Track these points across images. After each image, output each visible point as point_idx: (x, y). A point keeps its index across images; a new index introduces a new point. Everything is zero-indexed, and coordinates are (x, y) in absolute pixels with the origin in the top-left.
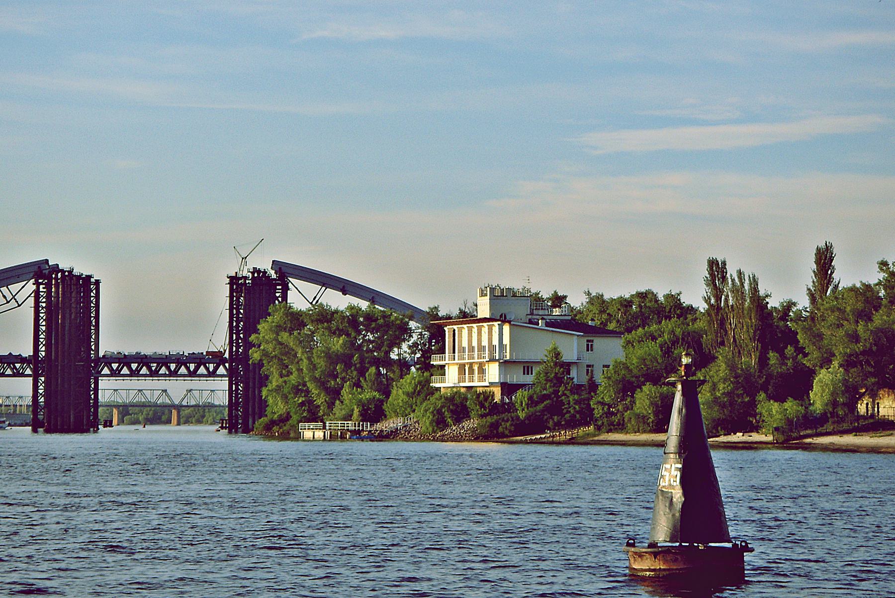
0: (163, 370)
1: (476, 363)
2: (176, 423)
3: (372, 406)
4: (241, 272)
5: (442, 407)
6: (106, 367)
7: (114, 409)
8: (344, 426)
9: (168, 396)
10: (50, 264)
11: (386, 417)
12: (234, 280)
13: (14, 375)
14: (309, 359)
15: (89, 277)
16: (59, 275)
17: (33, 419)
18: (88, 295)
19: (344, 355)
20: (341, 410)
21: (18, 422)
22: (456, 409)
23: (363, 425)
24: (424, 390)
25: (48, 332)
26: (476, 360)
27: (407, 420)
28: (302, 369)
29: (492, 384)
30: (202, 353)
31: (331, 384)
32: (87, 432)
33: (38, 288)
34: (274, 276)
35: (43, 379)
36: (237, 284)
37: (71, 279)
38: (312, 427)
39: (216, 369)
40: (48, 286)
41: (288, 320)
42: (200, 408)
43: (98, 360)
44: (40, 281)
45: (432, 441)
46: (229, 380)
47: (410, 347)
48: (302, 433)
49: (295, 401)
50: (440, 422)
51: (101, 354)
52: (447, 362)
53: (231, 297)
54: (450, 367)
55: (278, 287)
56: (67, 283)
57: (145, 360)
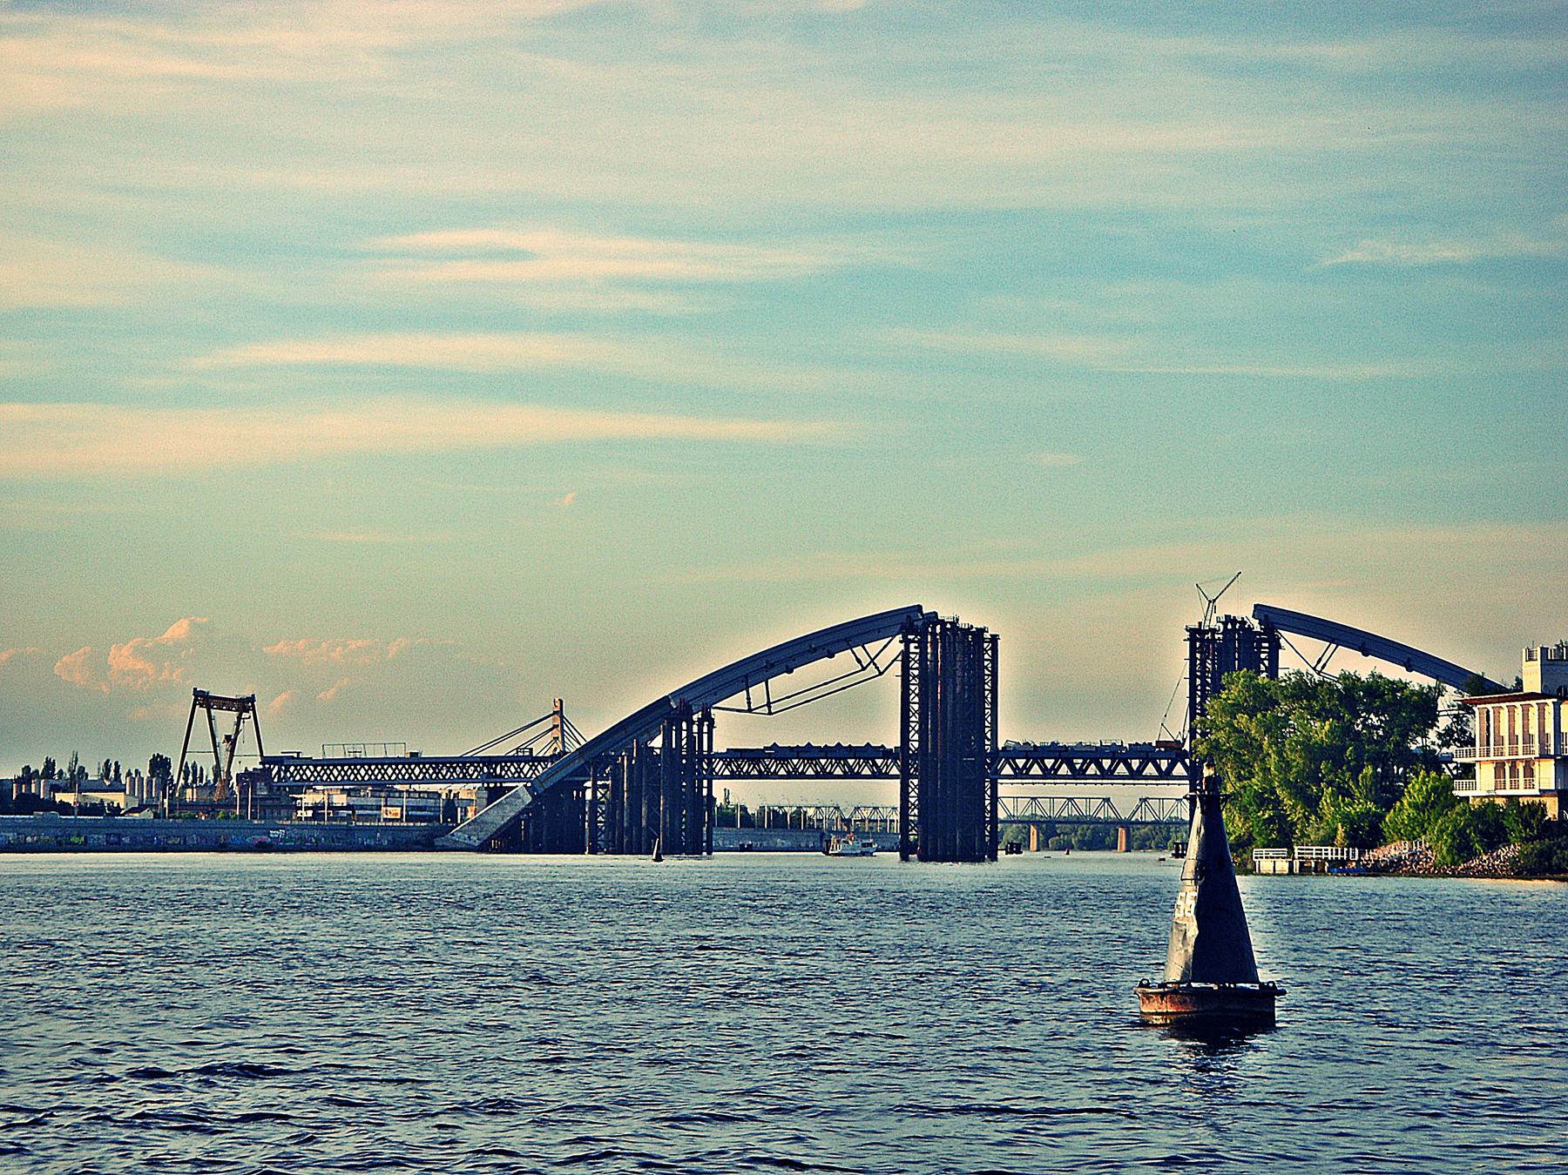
0: (1092, 769)
1: (1521, 760)
2: (1124, 848)
3: (1365, 824)
4: (1207, 623)
5: (1467, 826)
6: (1036, 765)
7: (1032, 827)
8: (1321, 854)
9: (1112, 807)
10: (924, 612)
11: (1385, 840)
12: (1196, 635)
13: (873, 776)
14: (1279, 753)
15: (983, 631)
16: (938, 627)
17: (901, 842)
18: (979, 657)
19: (1331, 746)
20: (1318, 829)
21: (888, 845)
22: (1487, 829)
23: (1348, 852)
24: (1442, 798)
25: (922, 713)
26: (1521, 756)
27: (1416, 845)
28: (1270, 769)
29: (1543, 792)
30: (1150, 744)
31: (1312, 790)
32: (979, 862)
33: (907, 647)
34: (1257, 628)
35: (916, 782)
36: (1202, 640)
37: (955, 635)
38: (1271, 854)
39: (1171, 767)
40: (922, 645)
41: (1250, 696)
42: (1162, 826)
43: (996, 754)
44: (911, 637)
45: (1451, 876)
46: (1190, 784)
47: (1440, 736)
48: (1257, 863)
49: (1259, 817)
50: (1462, 849)
51: (1000, 746)
52: (1478, 758)
53: (1192, 659)
54: (1482, 765)
55: (1264, 645)
56: (950, 639)
57: (1065, 755)
